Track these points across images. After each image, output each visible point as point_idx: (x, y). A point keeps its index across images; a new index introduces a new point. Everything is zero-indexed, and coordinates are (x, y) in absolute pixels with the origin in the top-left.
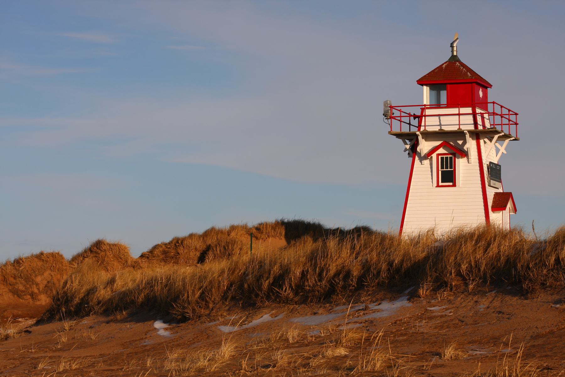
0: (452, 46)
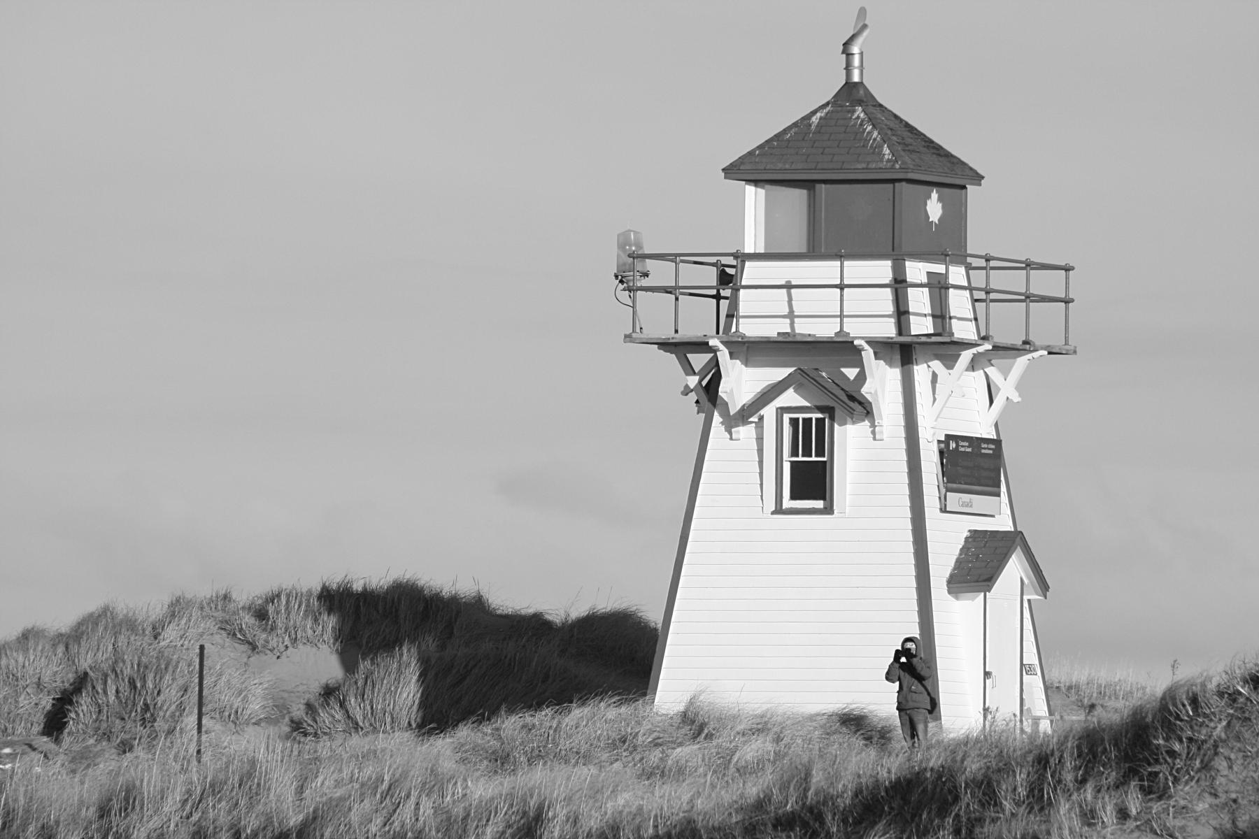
0: (849, 55)
